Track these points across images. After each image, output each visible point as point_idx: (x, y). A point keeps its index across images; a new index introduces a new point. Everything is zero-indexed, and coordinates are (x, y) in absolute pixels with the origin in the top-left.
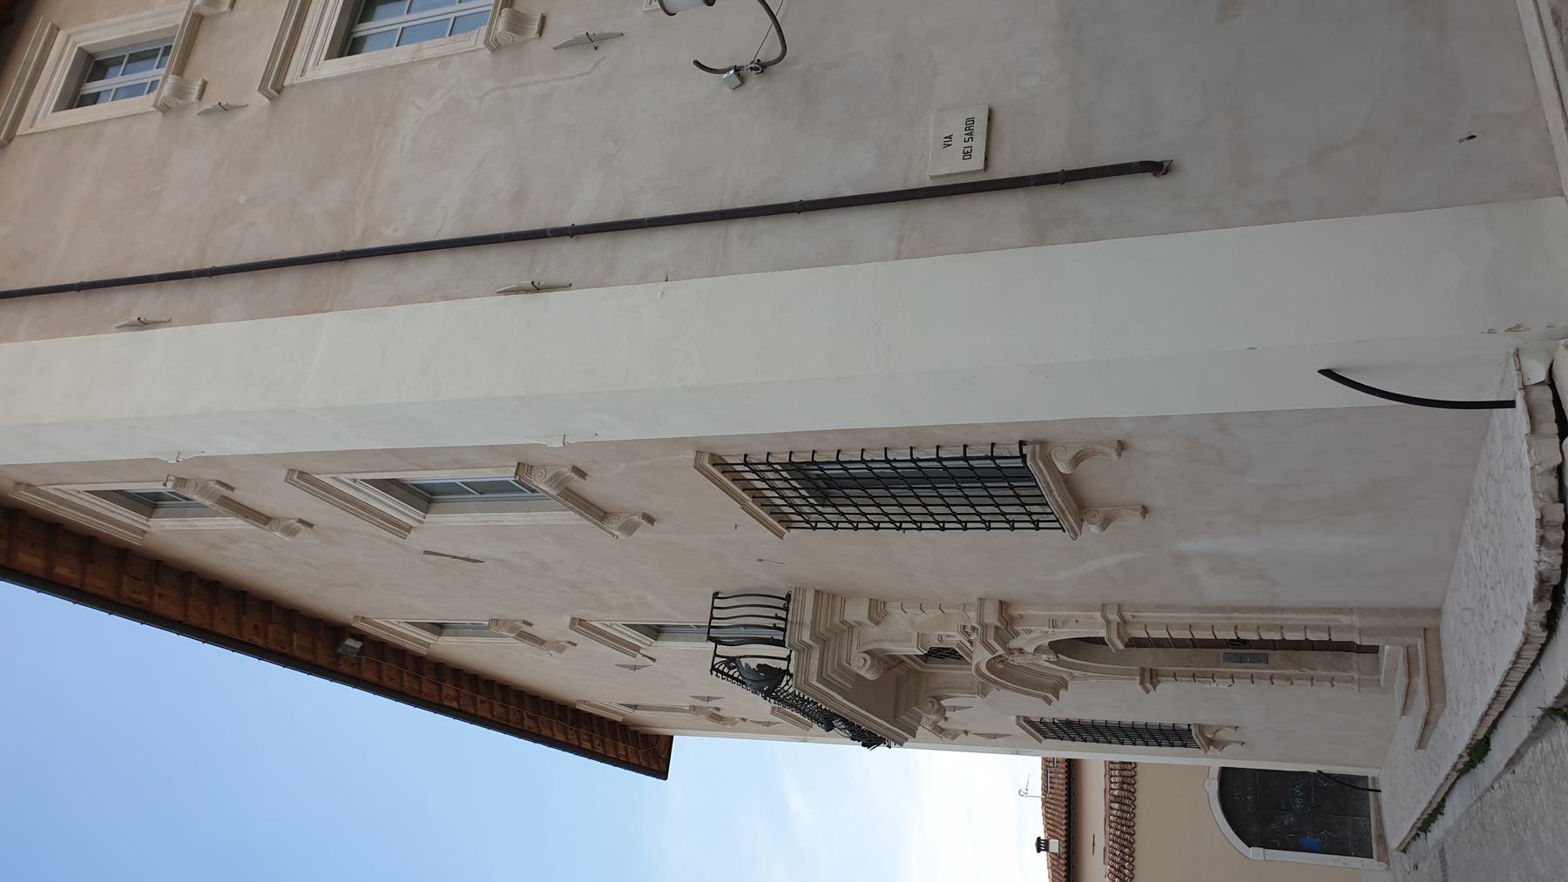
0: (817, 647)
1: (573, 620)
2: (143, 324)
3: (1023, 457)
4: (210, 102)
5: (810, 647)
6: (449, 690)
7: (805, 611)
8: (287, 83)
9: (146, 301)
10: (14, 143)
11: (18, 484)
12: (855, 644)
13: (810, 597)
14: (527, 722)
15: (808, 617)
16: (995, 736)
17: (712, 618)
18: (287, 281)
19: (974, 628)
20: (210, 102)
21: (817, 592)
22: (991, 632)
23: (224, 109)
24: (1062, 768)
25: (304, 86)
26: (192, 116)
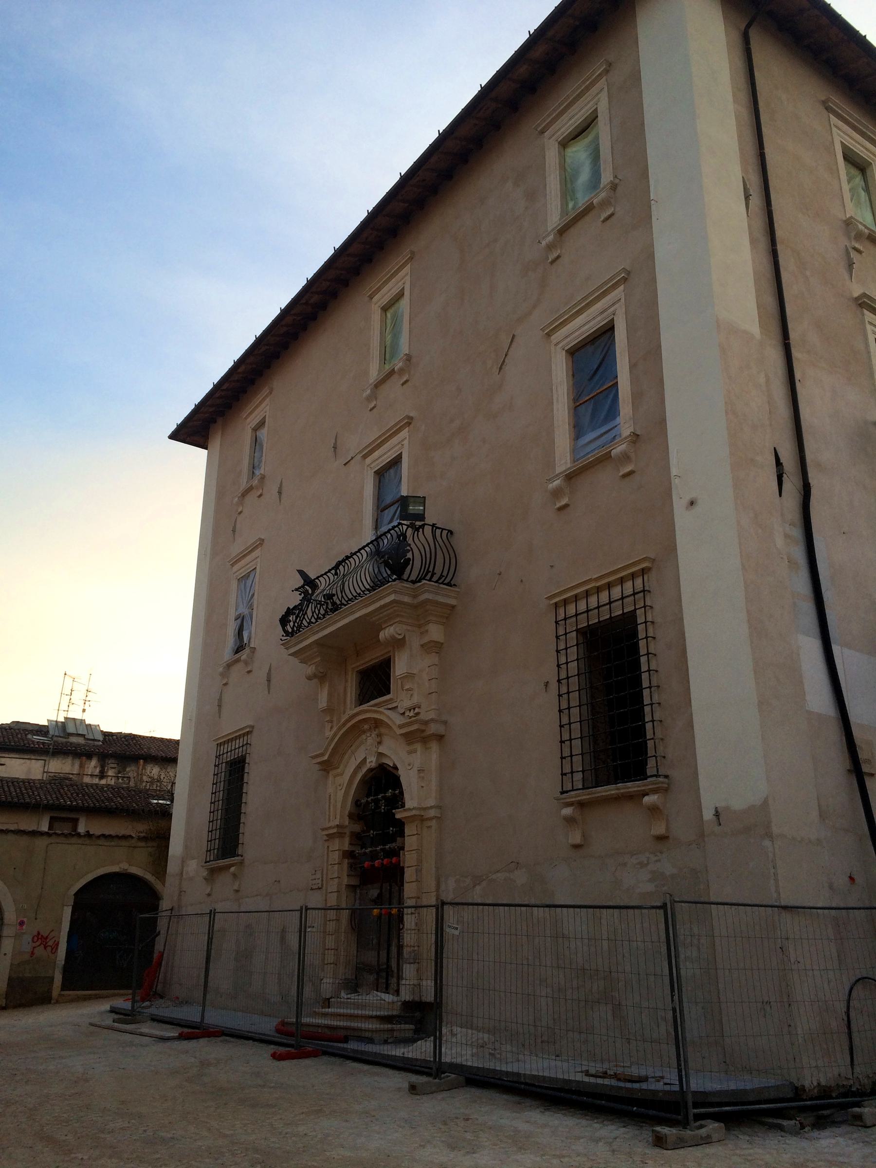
0: (415, 601)
1: (412, 418)
2: (747, 197)
3: (657, 776)
4: (853, 254)
5: (415, 597)
6: (315, 299)
7: (445, 597)
8: (865, 311)
9: (756, 200)
10: (825, 111)
11: (610, 65)
12: (409, 628)
13: (452, 602)
14: (263, 349)
15: (441, 599)
16: (220, 706)
17: (443, 529)
18: (770, 301)
19: (417, 714)
20: (853, 254)
21: (453, 607)
22: (423, 728)
23: (850, 265)
24: (170, 755)
25: (863, 322)
26: (843, 242)
